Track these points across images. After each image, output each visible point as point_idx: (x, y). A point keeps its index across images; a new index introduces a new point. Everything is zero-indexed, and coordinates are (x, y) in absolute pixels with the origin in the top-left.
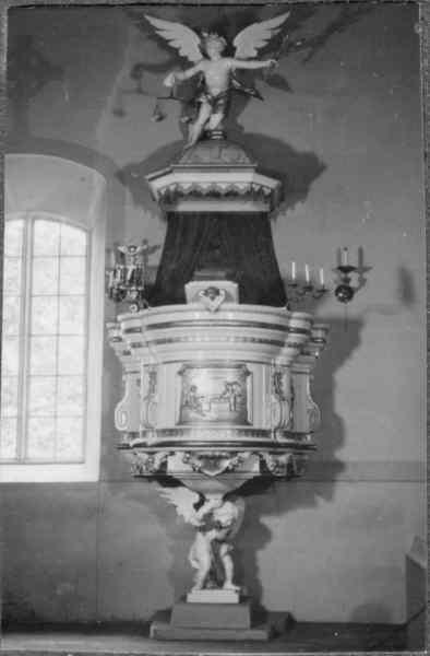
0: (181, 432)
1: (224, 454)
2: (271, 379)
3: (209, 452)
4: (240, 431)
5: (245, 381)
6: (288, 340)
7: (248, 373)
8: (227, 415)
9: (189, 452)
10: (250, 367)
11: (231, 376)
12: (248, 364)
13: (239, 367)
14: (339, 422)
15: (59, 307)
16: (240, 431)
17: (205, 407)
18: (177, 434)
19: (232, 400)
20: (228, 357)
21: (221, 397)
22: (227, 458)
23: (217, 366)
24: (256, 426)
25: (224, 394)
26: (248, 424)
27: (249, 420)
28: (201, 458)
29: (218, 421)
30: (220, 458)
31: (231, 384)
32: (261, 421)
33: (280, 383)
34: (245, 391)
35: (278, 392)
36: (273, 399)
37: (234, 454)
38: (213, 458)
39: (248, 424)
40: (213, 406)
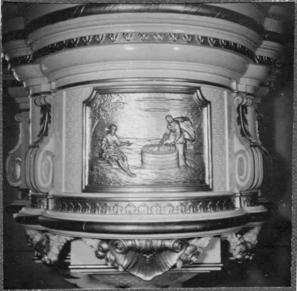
0: (93, 205)
1: (168, 244)
2: (235, 115)
3: (141, 241)
4: (196, 202)
5: (199, 116)
6: (259, 52)
7: (205, 103)
8: (174, 173)
9: (107, 241)
10: (208, 92)
11: (177, 107)
12: (204, 88)
13: (191, 91)
14: (41, 120)
15: (205, 72)
16: (196, 201)
17: (133, 160)
18: (85, 208)
19: (180, 148)
20: (130, 73)
21: (162, 142)
22: (173, 250)
23: (158, 90)
24: (217, 192)
25: (166, 136)
26: (207, 188)
27: (208, 181)
28: (127, 251)
29: (158, 185)
30: (163, 249)
31: (176, 121)
32: (224, 183)
33: (245, 121)
34: (199, 132)
35: (244, 133)
36: (238, 146)
37: (184, 243)
38: (150, 250)
39: (207, 188)
40: (149, 158)
